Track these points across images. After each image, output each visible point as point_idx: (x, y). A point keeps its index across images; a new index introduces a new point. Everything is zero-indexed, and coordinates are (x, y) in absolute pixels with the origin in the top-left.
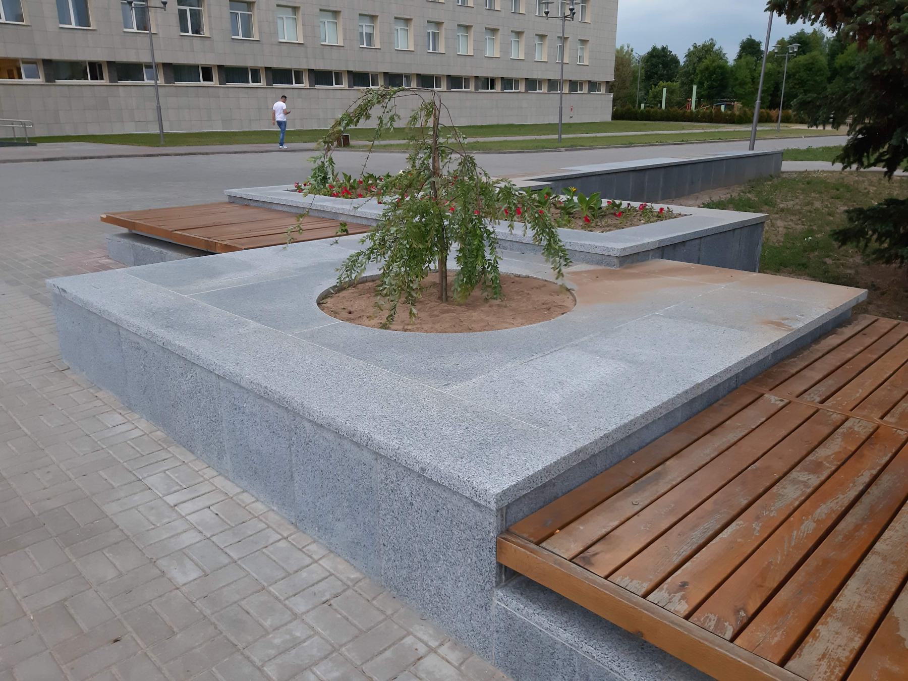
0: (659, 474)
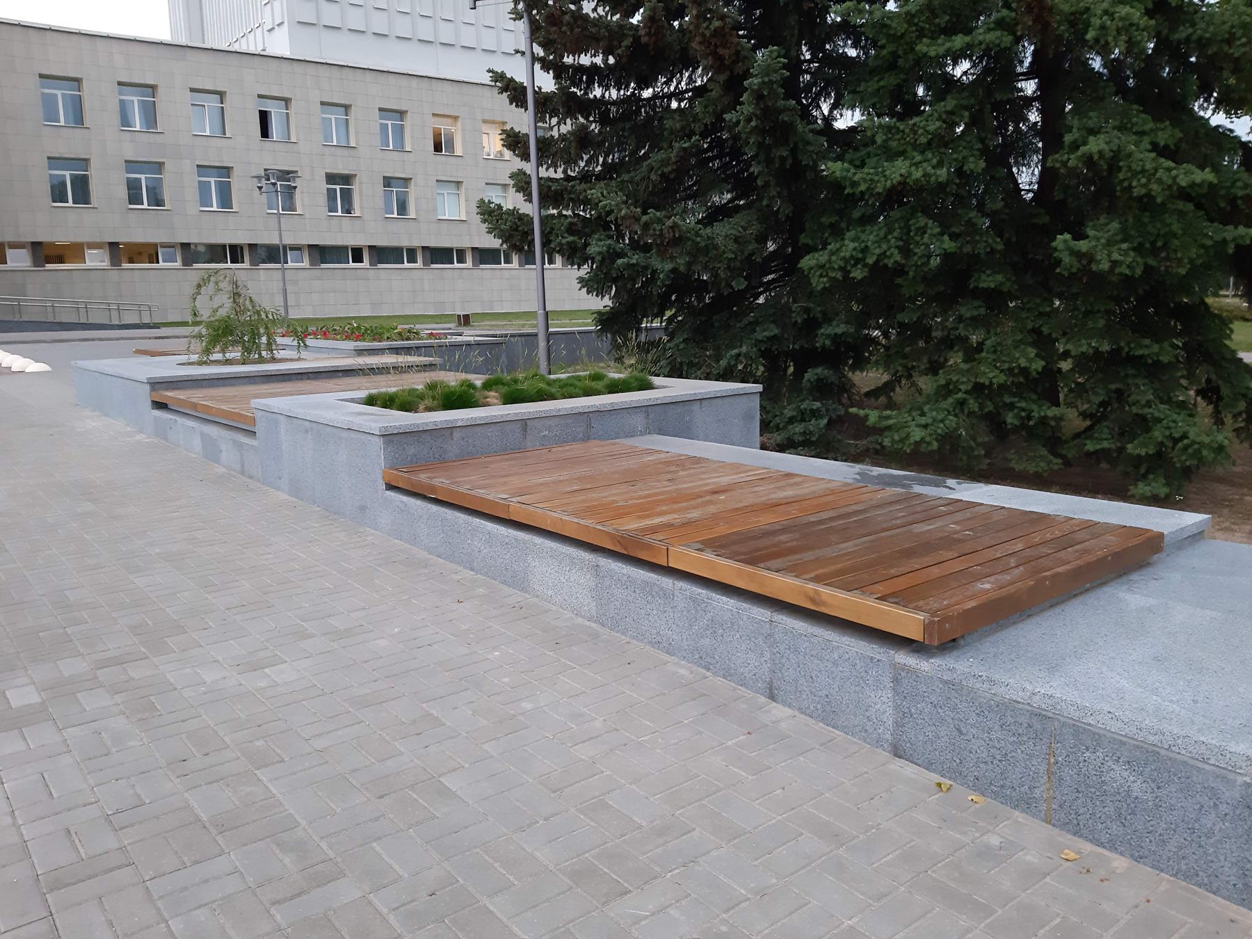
0: (813, 600)
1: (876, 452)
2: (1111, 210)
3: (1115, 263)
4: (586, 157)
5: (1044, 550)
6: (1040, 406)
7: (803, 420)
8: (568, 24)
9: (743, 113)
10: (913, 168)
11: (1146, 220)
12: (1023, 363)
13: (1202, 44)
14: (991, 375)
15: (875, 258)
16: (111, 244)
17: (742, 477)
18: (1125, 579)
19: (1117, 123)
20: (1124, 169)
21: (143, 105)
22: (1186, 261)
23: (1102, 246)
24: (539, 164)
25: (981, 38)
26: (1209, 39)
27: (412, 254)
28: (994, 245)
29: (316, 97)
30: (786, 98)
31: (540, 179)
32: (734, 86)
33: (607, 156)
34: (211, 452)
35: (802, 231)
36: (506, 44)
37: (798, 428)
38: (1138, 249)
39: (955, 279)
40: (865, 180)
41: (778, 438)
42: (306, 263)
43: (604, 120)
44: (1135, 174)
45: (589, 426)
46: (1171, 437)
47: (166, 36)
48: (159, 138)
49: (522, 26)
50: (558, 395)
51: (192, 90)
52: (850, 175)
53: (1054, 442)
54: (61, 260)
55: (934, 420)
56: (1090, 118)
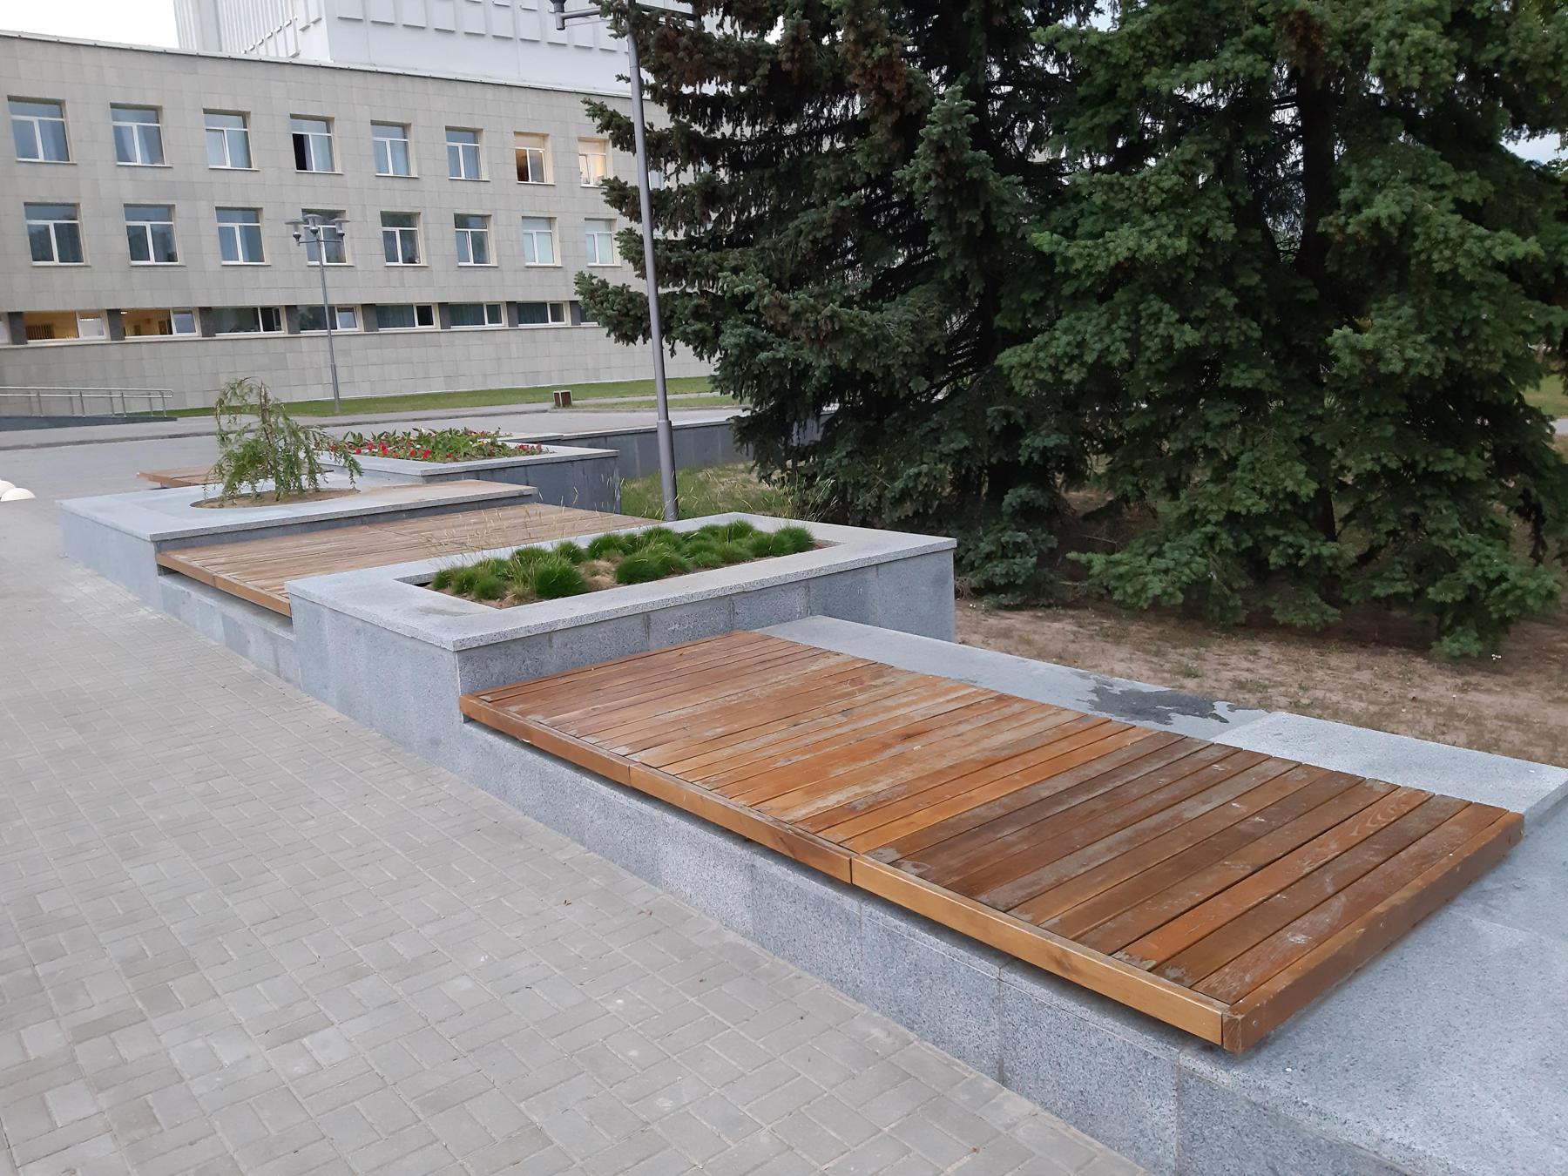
0: (1059, 963)
1: (1101, 598)
2: (1401, 286)
3: (1409, 363)
4: (714, 216)
5: (1368, 856)
6: (1312, 540)
7: (1004, 556)
8: (686, 48)
9: (917, 170)
10: (1144, 240)
11: (1447, 301)
12: (1290, 485)
13: (1518, 68)
14: (1250, 503)
15: (1094, 356)
16: (110, 312)
17: (940, 705)
18: (1474, 890)
19: (1409, 175)
20: (1422, 237)
21: (144, 131)
22: (1500, 355)
23: (1386, 337)
24: (653, 226)
25: (1228, 65)
26: (1527, 62)
27: (494, 312)
28: (1249, 333)
29: (365, 115)
30: (975, 148)
31: (655, 243)
32: (908, 129)
33: (741, 212)
34: (237, 642)
35: (998, 310)
36: (606, 66)
37: (998, 569)
38: (1438, 340)
39: (1194, 374)
40: (1080, 255)
41: (974, 580)
42: (360, 328)
43: (735, 165)
44: (1436, 244)
45: (733, 612)
46: (1484, 578)
47: (171, 43)
48: (166, 174)
49: (625, 44)
50: (690, 566)
51: (206, 111)
52: (1061, 249)
53: (1328, 582)
54: (47, 332)
55: (1177, 563)
56: (1373, 168)
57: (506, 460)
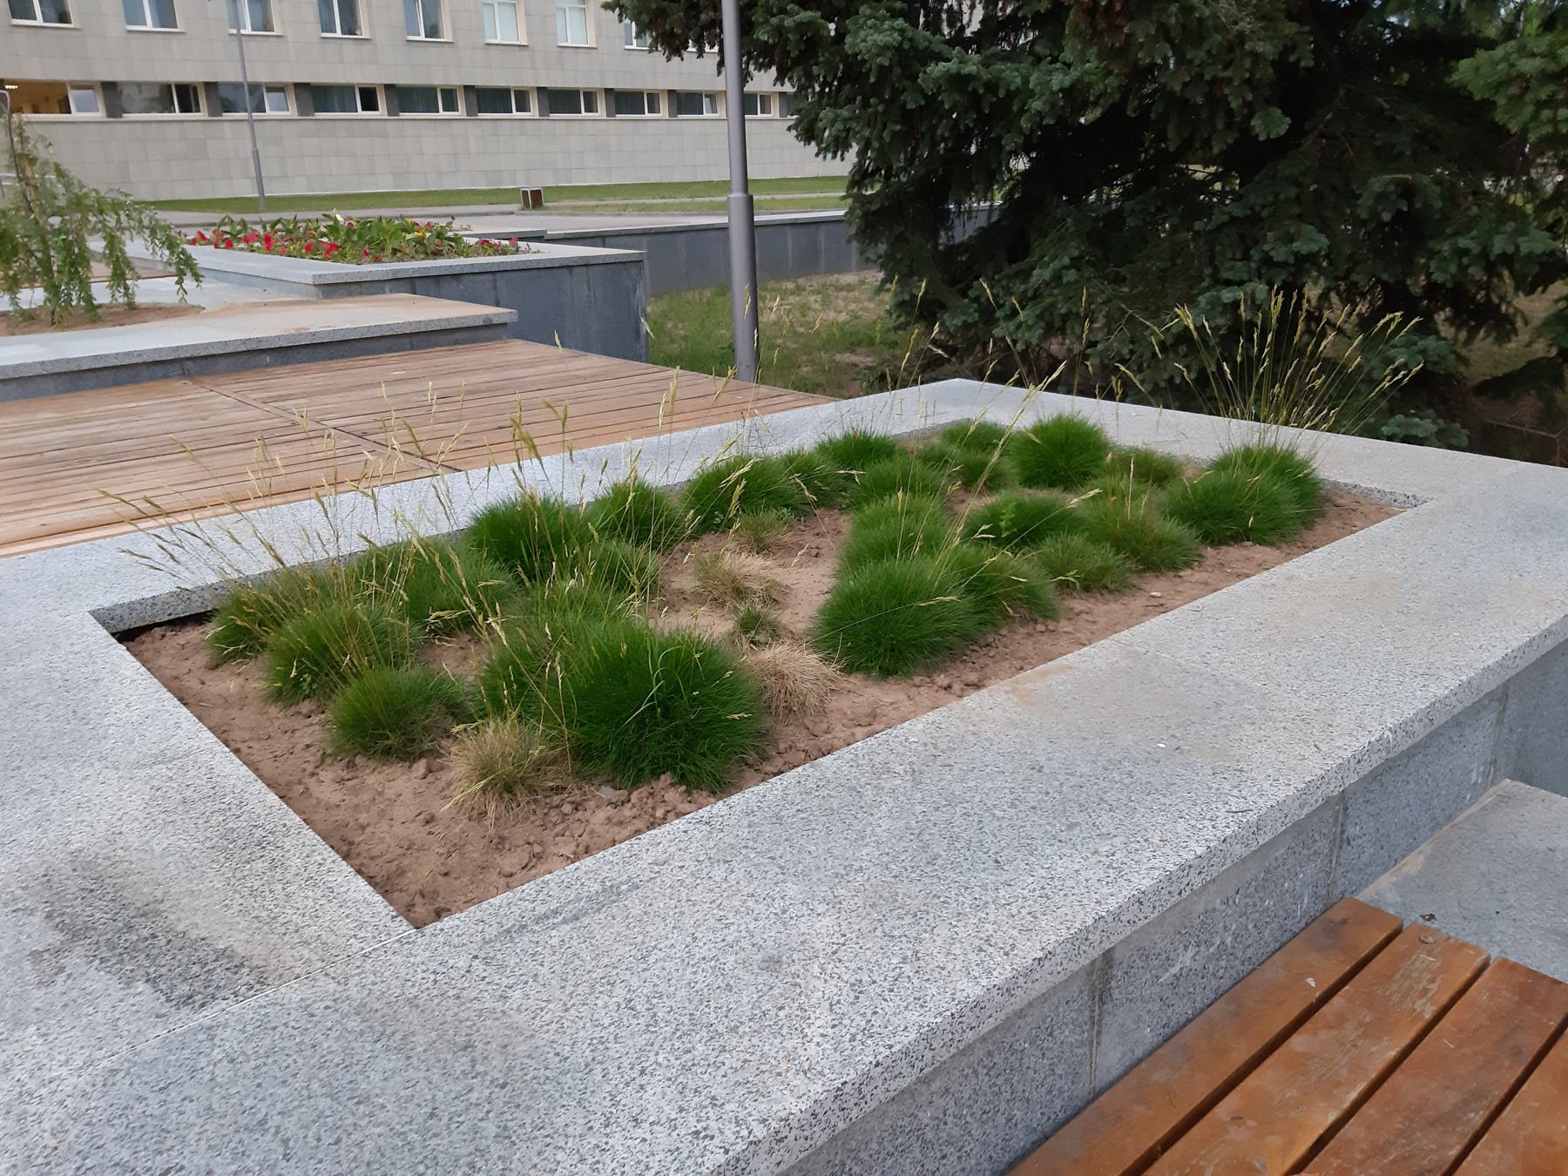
42: (292, 112)
57: (462, 261)
